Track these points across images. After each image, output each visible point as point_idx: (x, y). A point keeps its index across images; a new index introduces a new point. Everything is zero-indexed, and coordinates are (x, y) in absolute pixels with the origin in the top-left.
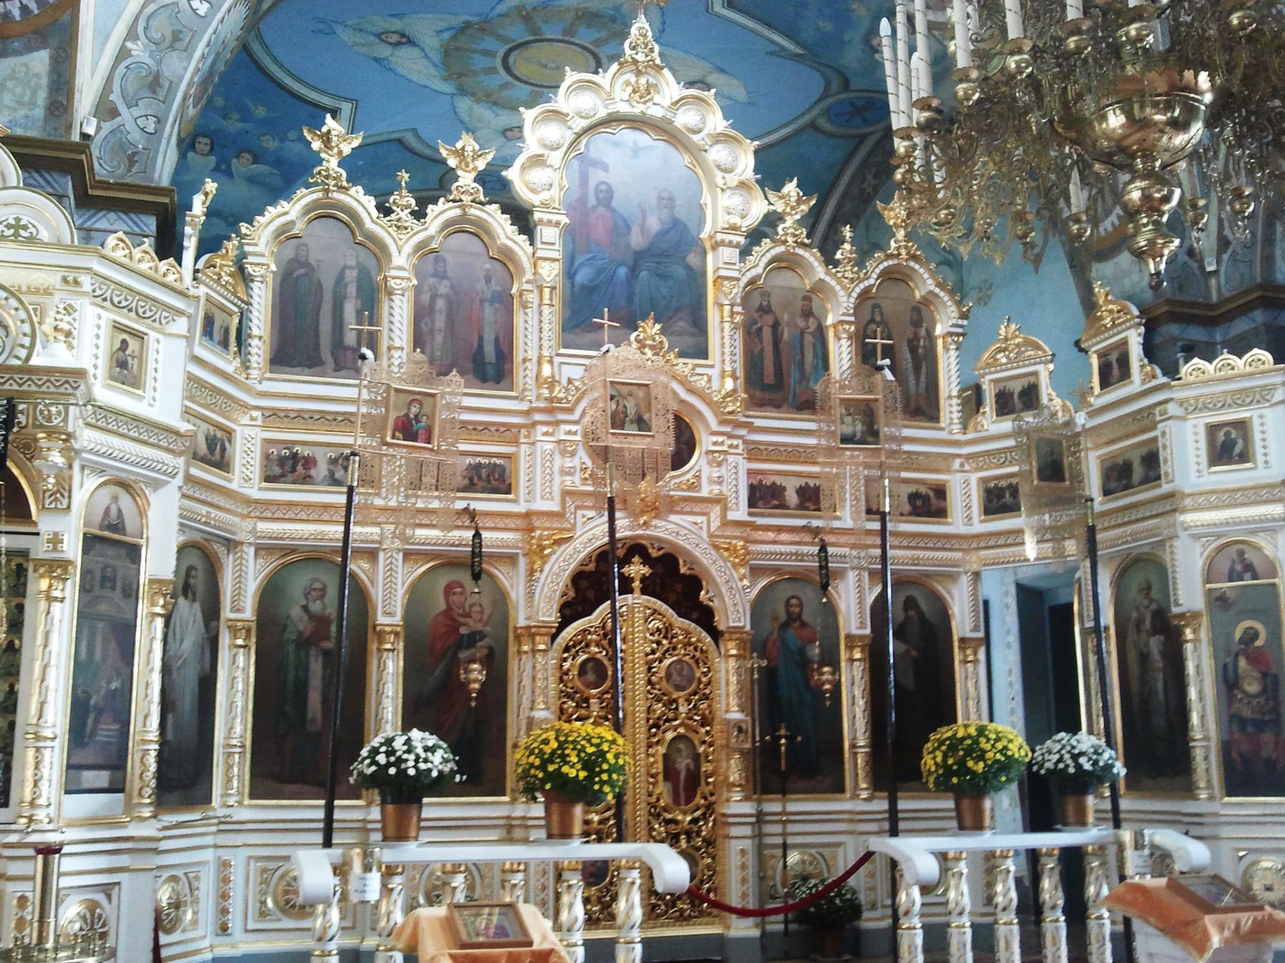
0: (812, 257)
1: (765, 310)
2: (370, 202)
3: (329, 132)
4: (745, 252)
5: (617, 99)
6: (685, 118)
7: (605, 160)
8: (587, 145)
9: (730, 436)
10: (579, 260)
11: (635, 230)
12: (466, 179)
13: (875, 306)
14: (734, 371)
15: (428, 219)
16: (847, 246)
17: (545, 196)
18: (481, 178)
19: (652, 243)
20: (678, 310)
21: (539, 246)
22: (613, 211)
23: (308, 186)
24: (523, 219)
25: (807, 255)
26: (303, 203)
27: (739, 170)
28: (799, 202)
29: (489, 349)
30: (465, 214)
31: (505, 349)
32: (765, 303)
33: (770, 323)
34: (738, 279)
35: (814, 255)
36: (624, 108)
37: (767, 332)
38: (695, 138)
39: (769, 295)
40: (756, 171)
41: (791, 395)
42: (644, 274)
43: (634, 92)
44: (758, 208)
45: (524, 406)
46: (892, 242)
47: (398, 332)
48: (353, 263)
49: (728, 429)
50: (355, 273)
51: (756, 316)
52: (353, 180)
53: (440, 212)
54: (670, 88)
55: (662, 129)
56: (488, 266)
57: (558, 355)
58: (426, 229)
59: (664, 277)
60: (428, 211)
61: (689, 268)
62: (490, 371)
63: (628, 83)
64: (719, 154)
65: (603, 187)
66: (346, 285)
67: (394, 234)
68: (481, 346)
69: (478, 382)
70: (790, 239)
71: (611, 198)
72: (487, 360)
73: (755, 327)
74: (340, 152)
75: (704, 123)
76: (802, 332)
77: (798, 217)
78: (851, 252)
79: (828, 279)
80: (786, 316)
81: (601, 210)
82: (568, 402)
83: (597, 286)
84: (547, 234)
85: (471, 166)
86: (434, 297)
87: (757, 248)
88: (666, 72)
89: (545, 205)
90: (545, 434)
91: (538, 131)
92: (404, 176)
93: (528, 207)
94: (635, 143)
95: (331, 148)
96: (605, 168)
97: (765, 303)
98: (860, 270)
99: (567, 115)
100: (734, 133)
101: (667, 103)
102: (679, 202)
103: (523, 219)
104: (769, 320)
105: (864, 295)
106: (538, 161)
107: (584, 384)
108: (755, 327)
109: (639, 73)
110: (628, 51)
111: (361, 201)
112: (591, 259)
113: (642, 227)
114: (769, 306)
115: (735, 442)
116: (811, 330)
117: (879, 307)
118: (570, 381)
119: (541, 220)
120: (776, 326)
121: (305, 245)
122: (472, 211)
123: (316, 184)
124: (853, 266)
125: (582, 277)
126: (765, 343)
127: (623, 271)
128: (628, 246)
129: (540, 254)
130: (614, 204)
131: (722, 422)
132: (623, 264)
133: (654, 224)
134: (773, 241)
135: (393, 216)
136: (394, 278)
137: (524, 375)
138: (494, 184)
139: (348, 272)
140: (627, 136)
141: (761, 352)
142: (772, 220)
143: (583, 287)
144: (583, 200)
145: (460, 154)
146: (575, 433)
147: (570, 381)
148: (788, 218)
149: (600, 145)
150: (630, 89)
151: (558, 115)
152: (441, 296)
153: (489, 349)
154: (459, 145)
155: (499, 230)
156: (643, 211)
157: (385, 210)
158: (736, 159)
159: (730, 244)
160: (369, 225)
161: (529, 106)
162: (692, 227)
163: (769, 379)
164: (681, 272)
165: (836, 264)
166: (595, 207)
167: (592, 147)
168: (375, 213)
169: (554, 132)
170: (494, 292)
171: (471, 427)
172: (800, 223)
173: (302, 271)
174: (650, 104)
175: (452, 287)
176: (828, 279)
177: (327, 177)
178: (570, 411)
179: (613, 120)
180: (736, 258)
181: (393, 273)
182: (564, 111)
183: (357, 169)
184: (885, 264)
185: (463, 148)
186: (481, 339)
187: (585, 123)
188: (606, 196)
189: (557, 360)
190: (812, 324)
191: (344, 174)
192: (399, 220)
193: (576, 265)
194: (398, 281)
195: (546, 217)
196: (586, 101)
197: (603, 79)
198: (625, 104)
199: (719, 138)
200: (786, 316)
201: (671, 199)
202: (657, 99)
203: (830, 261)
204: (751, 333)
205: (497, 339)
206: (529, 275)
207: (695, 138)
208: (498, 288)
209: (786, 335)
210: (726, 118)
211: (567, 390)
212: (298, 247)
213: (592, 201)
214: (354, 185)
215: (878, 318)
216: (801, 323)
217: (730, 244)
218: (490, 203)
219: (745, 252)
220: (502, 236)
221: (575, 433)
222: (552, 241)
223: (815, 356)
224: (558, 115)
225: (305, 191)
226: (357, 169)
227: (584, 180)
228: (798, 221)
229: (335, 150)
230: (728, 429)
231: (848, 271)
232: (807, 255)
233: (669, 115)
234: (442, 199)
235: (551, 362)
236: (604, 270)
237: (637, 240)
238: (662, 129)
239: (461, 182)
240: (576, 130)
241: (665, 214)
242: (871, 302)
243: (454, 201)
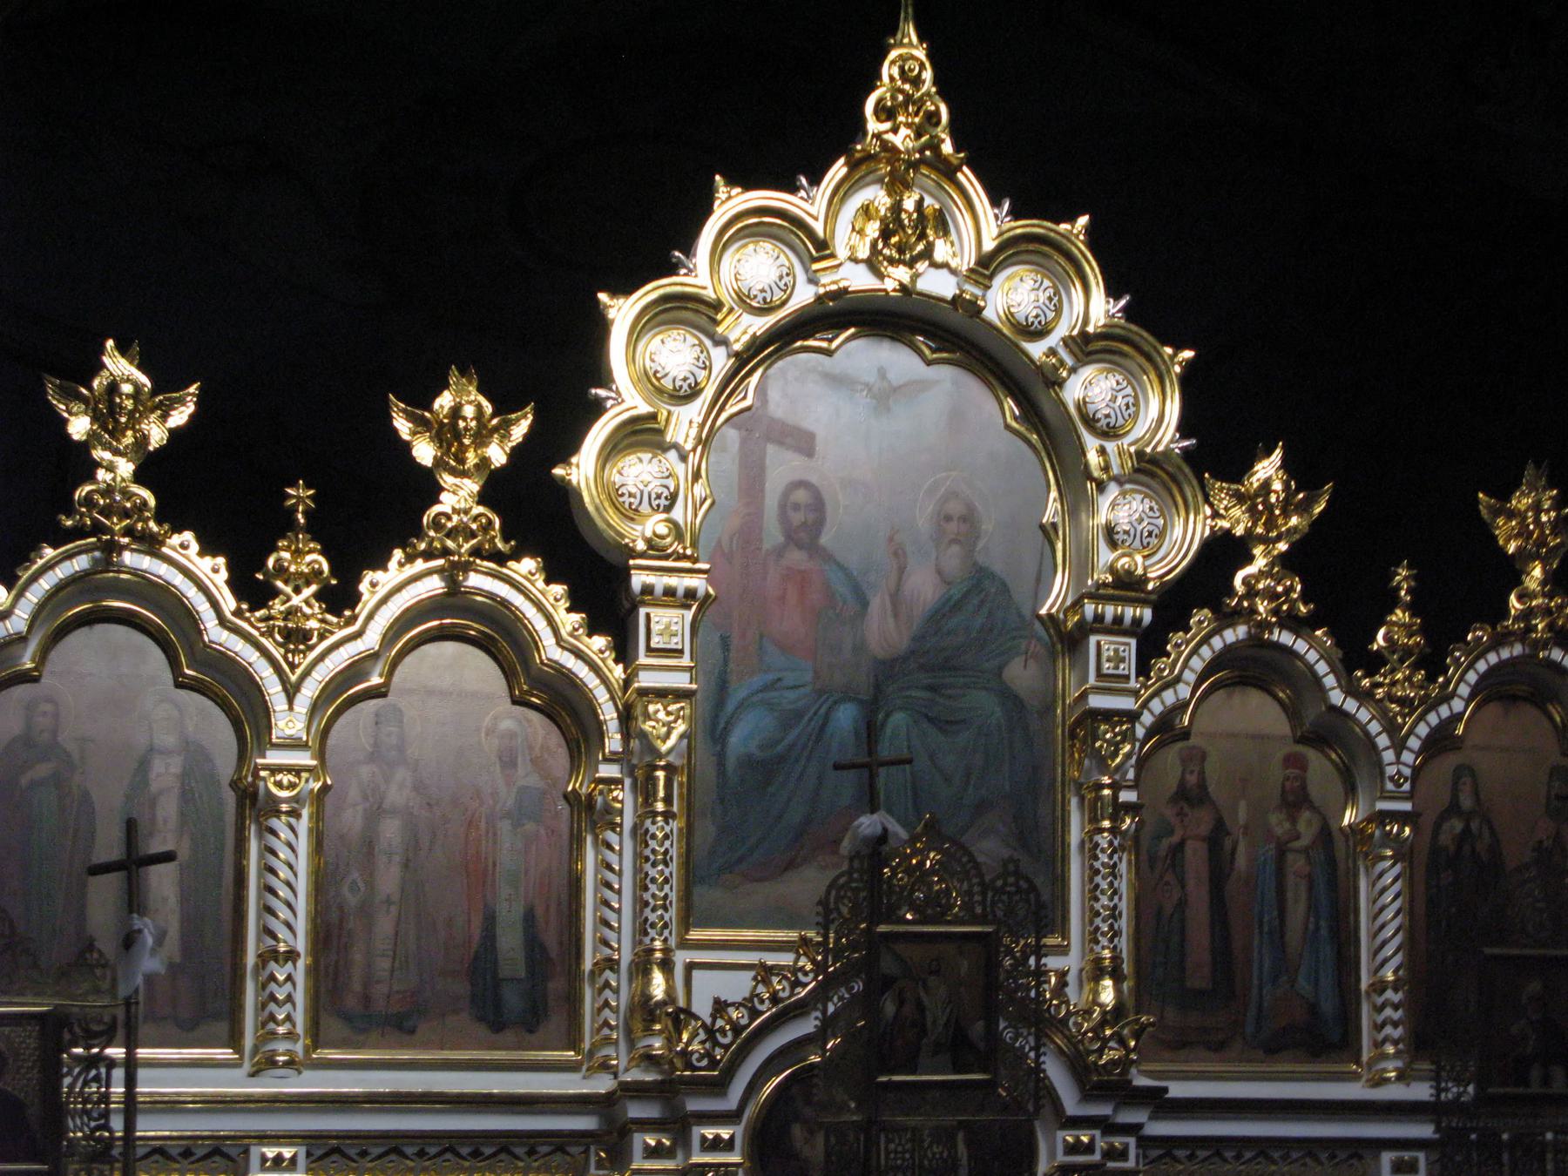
0: (1311, 651)
1: (1191, 796)
2: (214, 570)
3: (113, 388)
4: (1151, 645)
5: (842, 253)
6: (1014, 295)
7: (808, 424)
8: (761, 390)
9: (1108, 1126)
10: (738, 693)
11: (878, 603)
12: (458, 496)
13: (1459, 772)
14: (1116, 959)
15: (363, 610)
16: (1399, 615)
17: (655, 525)
18: (496, 490)
19: (919, 638)
20: (981, 807)
21: (643, 659)
22: (827, 557)
23: (59, 537)
24: (602, 587)
25: (1301, 646)
26: (45, 584)
27: (1140, 430)
28: (1287, 507)
29: (510, 942)
30: (454, 587)
31: (551, 939)
32: (1192, 779)
33: (1205, 829)
34: (1133, 717)
35: (1314, 643)
36: (858, 279)
37: (1196, 857)
38: (1037, 350)
39: (1204, 757)
40: (1184, 429)
41: (1252, 1013)
42: (899, 719)
43: (886, 234)
44: (1186, 534)
45: (602, 1085)
46: (1514, 603)
47: (283, 913)
48: (169, 740)
49: (1104, 1110)
50: (175, 765)
51: (1169, 813)
52: (174, 515)
53: (397, 585)
54: (981, 222)
55: (952, 333)
56: (507, 724)
57: (684, 944)
58: (359, 635)
59: (945, 725)
60: (364, 587)
61: (1011, 699)
62: (513, 1000)
63: (866, 211)
64: (1091, 387)
65: (801, 496)
66: (153, 802)
67: (277, 653)
68: (489, 936)
69: (482, 1031)
70: (1262, 607)
71: (817, 525)
72: (505, 972)
73: (1165, 843)
74: (143, 440)
75: (1058, 311)
76: (1282, 852)
77: (1282, 546)
78: (1408, 630)
79: (1351, 705)
80: (1242, 814)
81: (797, 557)
82: (713, 1064)
83: (781, 759)
84: (665, 624)
85: (472, 458)
86: (376, 813)
87: (1178, 637)
88: (967, 177)
89: (655, 547)
90: (653, 1153)
91: (641, 350)
92: (300, 495)
93: (613, 558)
94: (882, 373)
95: (116, 433)
96: (804, 443)
97: (1192, 779)
98: (1431, 678)
99: (717, 306)
100: (1022, 227)
101: (966, 261)
102: (987, 526)
103: (602, 587)
104: (1201, 821)
105: (1439, 742)
106: (641, 434)
107: (755, 1013)
108: (1165, 843)
109: (897, 184)
110: (873, 126)
111: (192, 568)
112: (766, 688)
113: (896, 597)
114: (1202, 785)
115: (1117, 1142)
116: (1304, 842)
117: (1471, 771)
118: (720, 1007)
119: (648, 590)
120: (1217, 838)
121: (50, 700)
122: (474, 580)
123: (78, 532)
124: (1415, 667)
125: (744, 737)
126: (1191, 884)
127: (846, 716)
128: (860, 648)
129: (646, 680)
130: (824, 540)
131: (1089, 1093)
132: (847, 696)
133: (924, 587)
134: (1217, 608)
135: (278, 606)
136: (275, 769)
137: (602, 1006)
138: (534, 511)
139: (158, 766)
140: (895, 360)
141: (1182, 904)
142: (1222, 553)
143: (748, 763)
144: (749, 533)
145: (447, 434)
146: (729, 1145)
147: (720, 1007)
148: (1258, 551)
149: (793, 385)
150: (873, 229)
151: (695, 312)
152: (394, 812)
153: (510, 942)
154: (444, 401)
155: (540, 624)
156: (899, 554)
157: (252, 589)
158: (1136, 405)
159: (1117, 627)
160: (214, 632)
161: (624, 288)
162: (1021, 592)
163: (1199, 979)
164: (985, 704)
165: (1374, 663)
166: (779, 552)
167: (774, 394)
168: (229, 603)
169: (675, 353)
170: (523, 790)
171: (465, 1151)
172: (1287, 563)
173: (42, 770)
174: (922, 266)
175: (419, 787)
176: (1351, 705)
177: (107, 511)
178: (718, 1086)
179: (838, 315)
180: (1130, 667)
181: (274, 758)
182: (709, 294)
183: (188, 486)
184: (1493, 658)
185: (456, 412)
186: (490, 920)
187: (760, 325)
188: (807, 519)
189: (681, 958)
190: (1307, 826)
191: (152, 502)
192: (290, 613)
193: (730, 707)
194: (286, 778)
195: (660, 582)
196: (759, 266)
197: (810, 204)
198: (862, 269)
199: (1086, 347)
200: (1242, 814)
201: (969, 518)
202: (942, 251)
203: (1355, 657)
204: (1156, 861)
205: (529, 918)
206: (614, 742)
207: (1037, 350)
208: (534, 781)
209: (1241, 861)
210: (1113, 292)
211: (711, 1032)
212: (30, 707)
213: (773, 534)
214: (178, 529)
215: (1466, 802)
216: (1278, 823)
217: (1117, 627)
218: (516, 556)
219: (1151, 645)
220: (548, 639)
221: (729, 1145)
222: (674, 643)
223: (1313, 907)
224: (695, 312)
225: (49, 553)
226: (188, 486)
227: (752, 478)
228: (1283, 557)
229: (129, 439)
230: (1104, 1110)
231: (1402, 680)
232: (1301, 646)
233: (971, 290)
234: (398, 554)
235: (667, 966)
236: (799, 715)
237: (884, 632)
238: (952, 333)
239: (447, 502)
240: (737, 347)
241: (953, 559)
242: (1451, 761)
243: (428, 555)
